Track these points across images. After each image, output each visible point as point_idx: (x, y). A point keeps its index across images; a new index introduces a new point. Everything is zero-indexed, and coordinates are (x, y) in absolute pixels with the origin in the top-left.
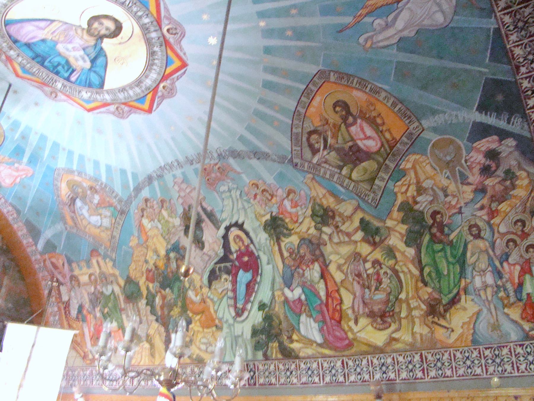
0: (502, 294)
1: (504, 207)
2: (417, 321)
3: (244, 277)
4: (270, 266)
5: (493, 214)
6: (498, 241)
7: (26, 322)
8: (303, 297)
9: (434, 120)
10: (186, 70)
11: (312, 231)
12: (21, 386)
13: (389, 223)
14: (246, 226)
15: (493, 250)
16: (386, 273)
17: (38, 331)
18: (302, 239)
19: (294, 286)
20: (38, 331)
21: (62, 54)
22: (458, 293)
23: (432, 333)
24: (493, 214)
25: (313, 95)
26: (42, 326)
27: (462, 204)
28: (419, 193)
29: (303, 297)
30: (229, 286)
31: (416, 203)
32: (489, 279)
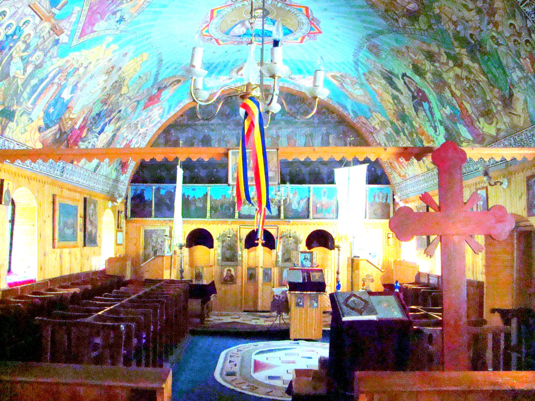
0: (530, 83)
2: (502, 113)
3: (426, 105)
4: (431, 95)
5: (496, 25)
6: (509, 43)
7: (343, 166)
8: (452, 112)
10: (311, 10)
11: (432, 68)
13: (457, 50)
14: (408, 74)
16: (474, 84)
17: (61, 272)
18: (432, 74)
19: (445, 106)
20: (61, 272)
23: (512, 119)
25: (57, 229)
27: (479, 25)
28: (456, 26)
29: (452, 112)
31: (459, 32)
32: (519, 74)
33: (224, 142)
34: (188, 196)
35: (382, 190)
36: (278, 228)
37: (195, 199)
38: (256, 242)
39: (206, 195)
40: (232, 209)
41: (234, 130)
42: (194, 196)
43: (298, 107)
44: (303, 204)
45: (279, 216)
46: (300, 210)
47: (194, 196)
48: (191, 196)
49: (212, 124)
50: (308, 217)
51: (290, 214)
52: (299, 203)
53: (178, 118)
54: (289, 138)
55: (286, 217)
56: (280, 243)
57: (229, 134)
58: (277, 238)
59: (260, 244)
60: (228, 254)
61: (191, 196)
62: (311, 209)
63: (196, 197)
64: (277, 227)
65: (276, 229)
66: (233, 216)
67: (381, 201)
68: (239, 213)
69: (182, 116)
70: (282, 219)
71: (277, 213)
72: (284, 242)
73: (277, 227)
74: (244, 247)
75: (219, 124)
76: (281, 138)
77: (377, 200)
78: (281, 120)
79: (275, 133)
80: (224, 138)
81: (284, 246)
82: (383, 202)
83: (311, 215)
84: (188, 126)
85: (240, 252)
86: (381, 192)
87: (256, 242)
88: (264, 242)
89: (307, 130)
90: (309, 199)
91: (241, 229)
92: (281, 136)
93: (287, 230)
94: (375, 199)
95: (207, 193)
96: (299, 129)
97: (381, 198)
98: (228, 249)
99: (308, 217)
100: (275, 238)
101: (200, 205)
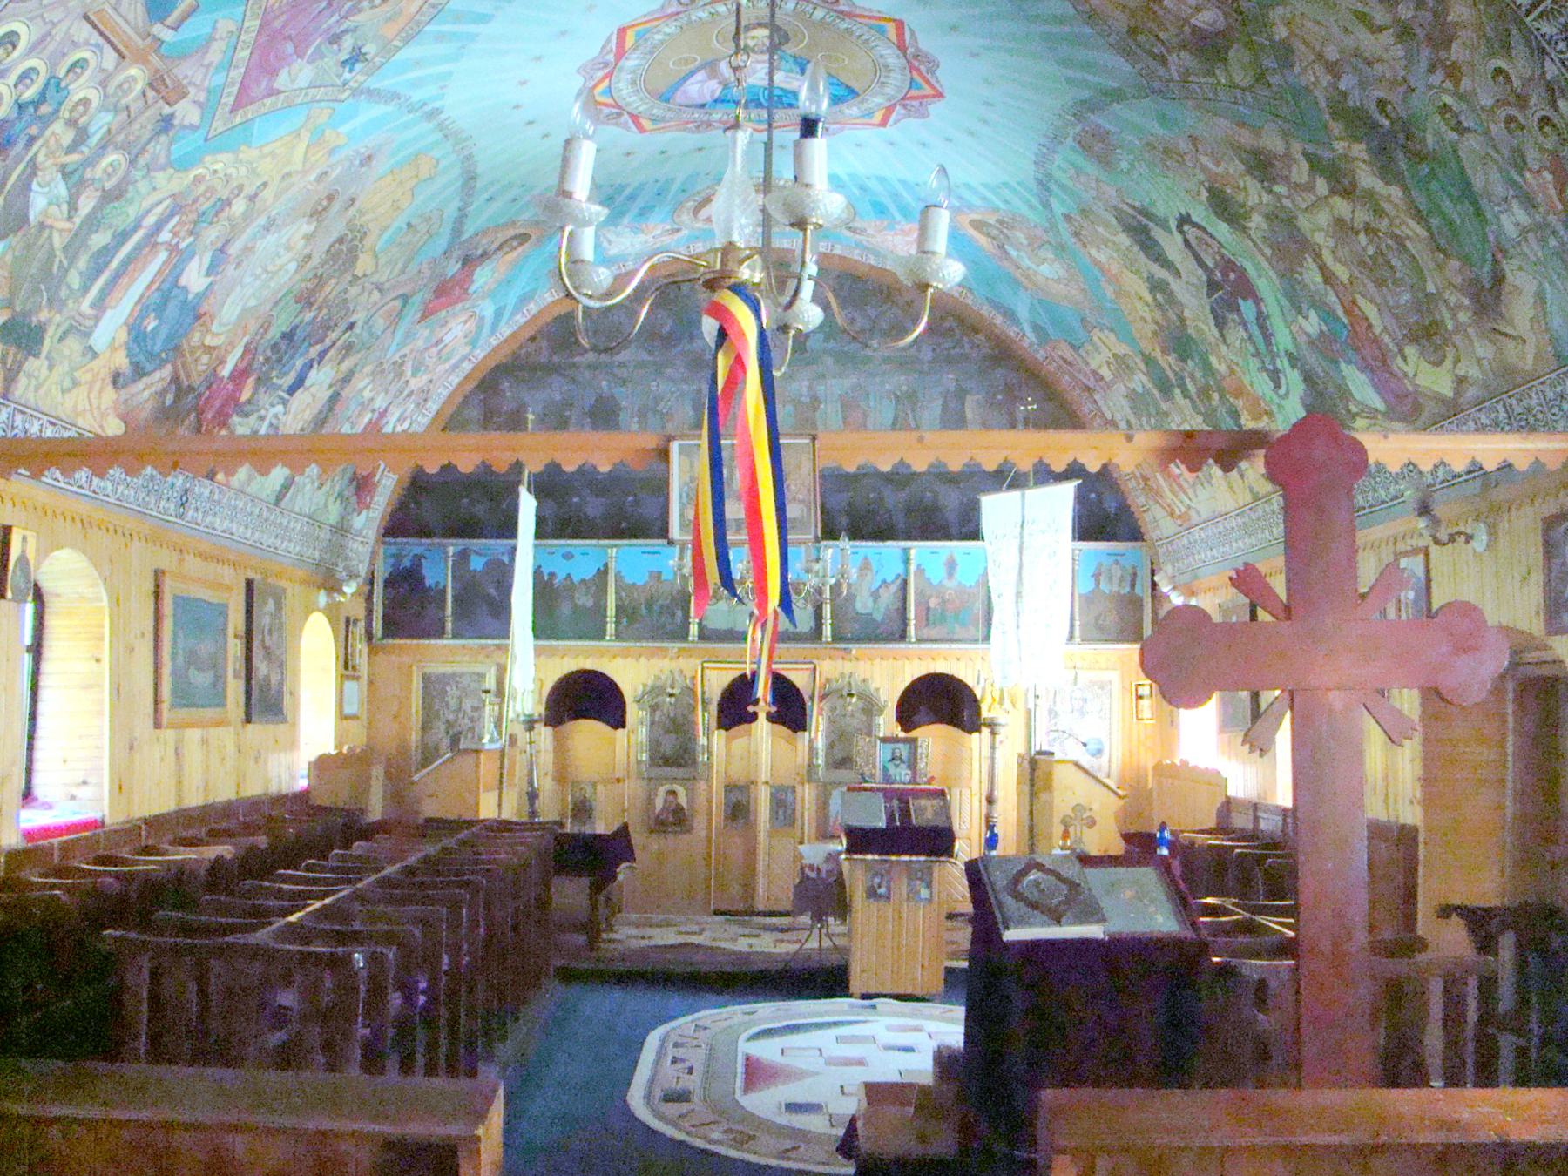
1: (1457, 52)
3: (1247, 308)
4: (1263, 280)
7: (1004, 488)
8: (1324, 328)
9: (16, 431)
10: (911, 30)
11: (1266, 198)
12: (1018, 614)
13: (1340, 146)
14: (1195, 218)
15: (1498, 151)
16: (1388, 246)
19: (1304, 310)
20: (1023, 496)
21: (13, 385)
22: (1495, 260)
24: (1453, 73)
26: (1029, 488)
29: (1324, 328)
30: (1243, 333)
31: (1344, 95)
33: (658, 417)
34: (552, 575)
35: (1119, 558)
36: (815, 669)
37: (572, 582)
38: (751, 709)
39: (603, 573)
40: (679, 613)
41: (685, 380)
42: (569, 576)
43: (872, 313)
44: (888, 597)
45: (817, 634)
46: (878, 617)
47: (569, 576)
48: (561, 576)
49: (621, 365)
50: (903, 637)
51: (850, 628)
52: (875, 595)
53: (521, 347)
54: (847, 405)
55: (837, 637)
56: (820, 714)
57: (672, 393)
58: (812, 698)
59: (762, 716)
60: (669, 745)
61: (561, 576)
62: (912, 614)
63: (576, 579)
64: (811, 666)
65: (808, 673)
66: (683, 635)
67: (1115, 588)
68: (700, 624)
69: (533, 339)
70: (827, 643)
71: (812, 624)
72: (833, 709)
73: (811, 666)
74: (714, 723)
75: (641, 365)
76: (822, 406)
77: (1104, 587)
78: (825, 351)
79: (805, 390)
80: (657, 404)
81: (831, 721)
82: (1122, 592)
83: (912, 630)
84: (552, 369)
85: (702, 740)
86: (1117, 562)
87: (751, 709)
88: (773, 709)
89: (900, 381)
90: (905, 583)
91: (706, 671)
92: (822, 399)
93: (842, 675)
94: (1098, 583)
95: (606, 565)
96: (878, 379)
97: (1116, 580)
98: (668, 732)
99: (903, 637)
100: (806, 697)
101: (586, 601)
